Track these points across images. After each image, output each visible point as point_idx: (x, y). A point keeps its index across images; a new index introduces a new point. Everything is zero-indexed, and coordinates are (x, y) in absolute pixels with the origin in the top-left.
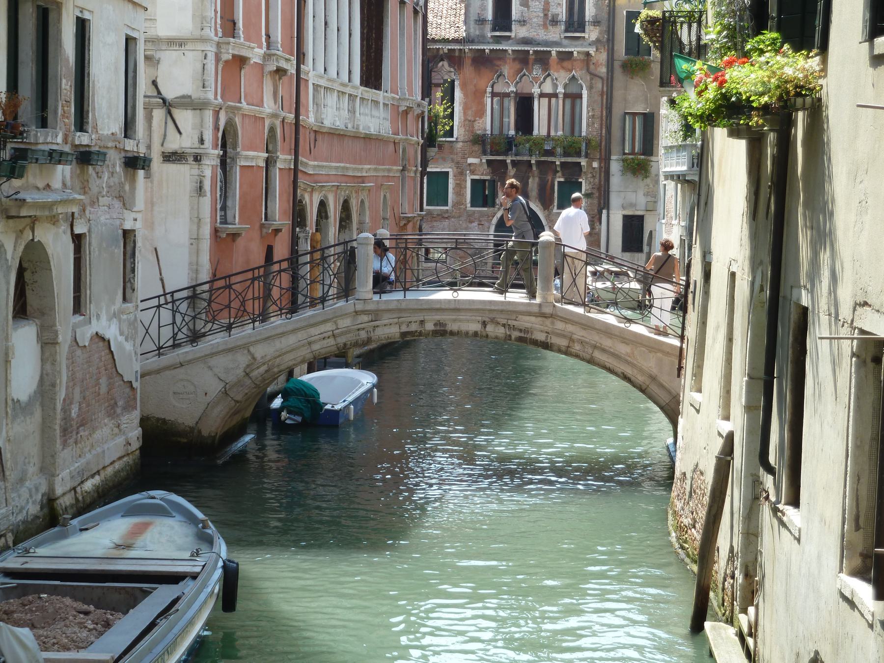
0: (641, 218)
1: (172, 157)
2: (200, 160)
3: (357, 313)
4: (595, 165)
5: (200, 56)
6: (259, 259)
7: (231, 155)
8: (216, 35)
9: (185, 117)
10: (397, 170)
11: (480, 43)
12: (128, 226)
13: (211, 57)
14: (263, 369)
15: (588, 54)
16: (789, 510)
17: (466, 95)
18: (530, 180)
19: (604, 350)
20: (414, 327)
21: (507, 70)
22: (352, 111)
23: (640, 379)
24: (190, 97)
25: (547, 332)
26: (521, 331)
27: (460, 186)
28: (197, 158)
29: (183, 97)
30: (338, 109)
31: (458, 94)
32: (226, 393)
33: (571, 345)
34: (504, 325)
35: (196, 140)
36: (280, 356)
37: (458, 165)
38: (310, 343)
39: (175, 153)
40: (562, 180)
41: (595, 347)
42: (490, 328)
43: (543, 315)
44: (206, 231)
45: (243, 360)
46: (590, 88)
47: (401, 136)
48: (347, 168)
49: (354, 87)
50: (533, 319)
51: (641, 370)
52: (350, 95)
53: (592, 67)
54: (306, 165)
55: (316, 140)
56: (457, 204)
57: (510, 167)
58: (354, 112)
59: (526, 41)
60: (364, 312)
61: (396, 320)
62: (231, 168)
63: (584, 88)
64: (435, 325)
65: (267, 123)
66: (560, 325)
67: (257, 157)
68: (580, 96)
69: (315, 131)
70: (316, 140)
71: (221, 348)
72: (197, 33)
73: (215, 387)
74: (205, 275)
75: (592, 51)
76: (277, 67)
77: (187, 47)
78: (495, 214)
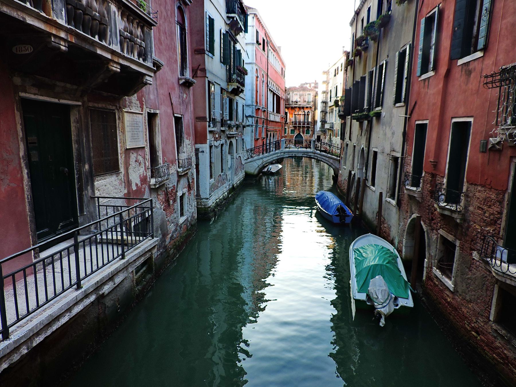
4: (312, 126)
6: (261, 144)
9: (250, 119)
13: (254, 108)
22: (275, 118)
27: (289, 131)
28: (252, 126)
31: (288, 114)
37: (288, 127)
41: (322, 158)
44: (253, 139)
45: (261, 161)
46: (311, 113)
56: (288, 134)
59: (300, 105)
60: (282, 153)
65: (263, 120)
66: (316, 155)
72: (252, 104)
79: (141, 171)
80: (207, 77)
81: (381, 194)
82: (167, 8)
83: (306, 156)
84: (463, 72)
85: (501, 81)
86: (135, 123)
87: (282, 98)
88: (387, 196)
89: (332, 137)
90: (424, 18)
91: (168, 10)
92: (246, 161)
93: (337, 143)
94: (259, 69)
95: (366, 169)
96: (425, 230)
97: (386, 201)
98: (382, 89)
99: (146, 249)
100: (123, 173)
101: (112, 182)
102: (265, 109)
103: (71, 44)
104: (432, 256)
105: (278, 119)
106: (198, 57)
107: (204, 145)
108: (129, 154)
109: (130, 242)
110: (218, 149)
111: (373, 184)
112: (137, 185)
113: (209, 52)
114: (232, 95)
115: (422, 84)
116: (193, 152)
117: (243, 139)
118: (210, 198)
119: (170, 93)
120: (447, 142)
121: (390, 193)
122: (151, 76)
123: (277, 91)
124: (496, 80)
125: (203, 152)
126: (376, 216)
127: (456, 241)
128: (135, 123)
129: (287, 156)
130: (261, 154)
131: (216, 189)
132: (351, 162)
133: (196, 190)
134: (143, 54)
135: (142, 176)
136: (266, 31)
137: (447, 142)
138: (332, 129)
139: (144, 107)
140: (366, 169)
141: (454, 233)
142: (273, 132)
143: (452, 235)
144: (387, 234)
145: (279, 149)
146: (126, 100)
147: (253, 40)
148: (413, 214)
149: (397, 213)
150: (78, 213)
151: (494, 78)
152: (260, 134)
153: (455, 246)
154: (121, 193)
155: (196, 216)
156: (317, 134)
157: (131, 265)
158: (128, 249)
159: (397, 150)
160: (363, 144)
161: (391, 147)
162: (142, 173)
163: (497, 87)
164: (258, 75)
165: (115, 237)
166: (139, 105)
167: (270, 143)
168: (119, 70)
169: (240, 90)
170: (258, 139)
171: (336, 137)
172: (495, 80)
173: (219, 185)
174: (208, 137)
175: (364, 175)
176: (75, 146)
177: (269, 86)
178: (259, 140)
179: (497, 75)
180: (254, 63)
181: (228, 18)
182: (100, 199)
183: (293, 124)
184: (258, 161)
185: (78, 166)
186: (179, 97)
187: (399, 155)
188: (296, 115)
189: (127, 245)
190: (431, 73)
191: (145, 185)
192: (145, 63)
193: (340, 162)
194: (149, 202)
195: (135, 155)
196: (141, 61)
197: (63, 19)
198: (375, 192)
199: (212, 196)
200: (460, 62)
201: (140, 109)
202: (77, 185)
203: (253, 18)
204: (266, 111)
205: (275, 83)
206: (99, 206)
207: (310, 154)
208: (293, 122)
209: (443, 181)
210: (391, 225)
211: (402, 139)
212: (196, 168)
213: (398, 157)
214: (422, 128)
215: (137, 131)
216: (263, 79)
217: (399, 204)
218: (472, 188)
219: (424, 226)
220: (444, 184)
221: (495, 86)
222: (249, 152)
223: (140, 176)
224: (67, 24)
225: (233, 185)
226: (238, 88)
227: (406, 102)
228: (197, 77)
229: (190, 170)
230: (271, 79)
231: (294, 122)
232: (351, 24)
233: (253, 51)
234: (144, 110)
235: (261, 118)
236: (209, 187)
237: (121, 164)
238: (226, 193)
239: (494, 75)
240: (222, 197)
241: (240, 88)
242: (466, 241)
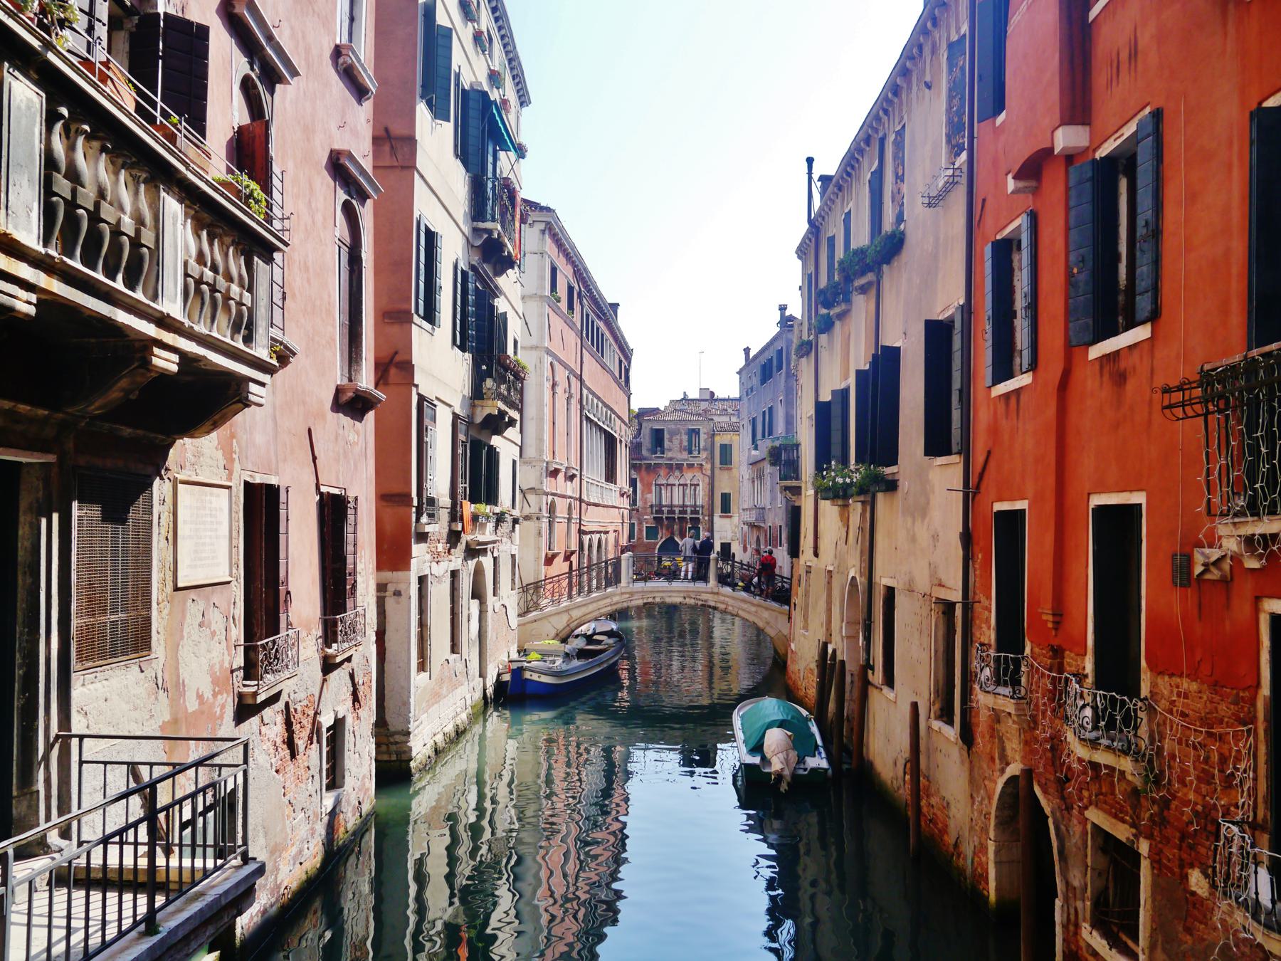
0: (729, 544)
1: (527, 518)
3: (622, 594)
4: (707, 518)
11: (648, 460)
15: (701, 465)
17: (643, 485)
19: (744, 610)
20: (650, 600)
21: (662, 472)
27: (640, 530)
31: (639, 485)
37: (639, 519)
42: (687, 600)
43: (712, 593)
53: (704, 472)
56: (639, 539)
59: (671, 459)
68: (698, 485)
75: (704, 463)
79: (215, 654)
80: (417, 386)
81: (915, 706)
82: (313, 205)
84: (1106, 377)
85: (1205, 401)
86: (208, 512)
87: (621, 441)
88: (932, 715)
90: (990, 245)
91: (317, 210)
95: (868, 639)
96: (1047, 811)
99: (223, 899)
100: (162, 660)
101: (126, 687)
102: (575, 472)
103: (43, 297)
104: (1075, 888)
106: (395, 330)
107: (400, 574)
108: (184, 603)
109: (174, 876)
110: (443, 584)
111: (889, 680)
112: (200, 697)
113: (424, 318)
114: (486, 432)
115: (1001, 407)
116: (370, 595)
119: (310, 431)
120: (1084, 560)
121: (937, 706)
122: (263, 385)
124: (1194, 399)
126: (905, 773)
127: (1138, 840)
128: (208, 512)
130: (565, 598)
131: (433, 704)
132: (823, 617)
134: (245, 326)
135: (217, 666)
136: (576, 266)
137: (1084, 560)
139: (237, 466)
140: (868, 639)
141: (1131, 817)
142: (598, 536)
143: (1123, 821)
144: (940, 825)
146: (186, 449)
148: (1008, 764)
149: (962, 762)
150: (14, 787)
151: (1187, 393)
153: (1137, 856)
154: (152, 722)
156: (721, 539)
157: (172, 952)
158: (167, 899)
159: (950, 583)
160: (854, 566)
161: (931, 576)
162: (216, 661)
163: (1199, 415)
165: (128, 861)
166: (222, 463)
167: (579, 569)
168: (174, 368)
169: (507, 420)
172: (1190, 399)
173: (444, 691)
175: (862, 655)
176: (24, 581)
179: (1194, 385)
181: (476, 231)
182: (85, 740)
183: (652, 513)
184: (556, 618)
185: (27, 641)
186: (336, 439)
187: (956, 596)
188: (660, 485)
189: (164, 887)
190: (1023, 380)
191: (225, 695)
192: (248, 347)
194: (241, 747)
195: (201, 605)
196: (240, 345)
197: (30, 231)
198: (895, 702)
200: (1096, 352)
201: (224, 474)
202: (19, 698)
203: (543, 232)
204: (578, 476)
206: (81, 763)
208: (651, 506)
209: (1084, 668)
210: (948, 797)
211: (960, 552)
212: (377, 642)
213: (954, 604)
214: (1010, 524)
215: (211, 537)
217: (967, 736)
218: (1164, 683)
219: (1043, 802)
220: (1086, 676)
221: (1190, 413)
222: (531, 591)
223: (211, 667)
224: (41, 243)
227: (965, 452)
228: (386, 384)
229: (360, 648)
230: (589, 389)
231: (656, 506)
232: (802, 252)
234: (235, 475)
237: (158, 633)
239: (1185, 387)
241: (507, 413)
242: (1167, 840)
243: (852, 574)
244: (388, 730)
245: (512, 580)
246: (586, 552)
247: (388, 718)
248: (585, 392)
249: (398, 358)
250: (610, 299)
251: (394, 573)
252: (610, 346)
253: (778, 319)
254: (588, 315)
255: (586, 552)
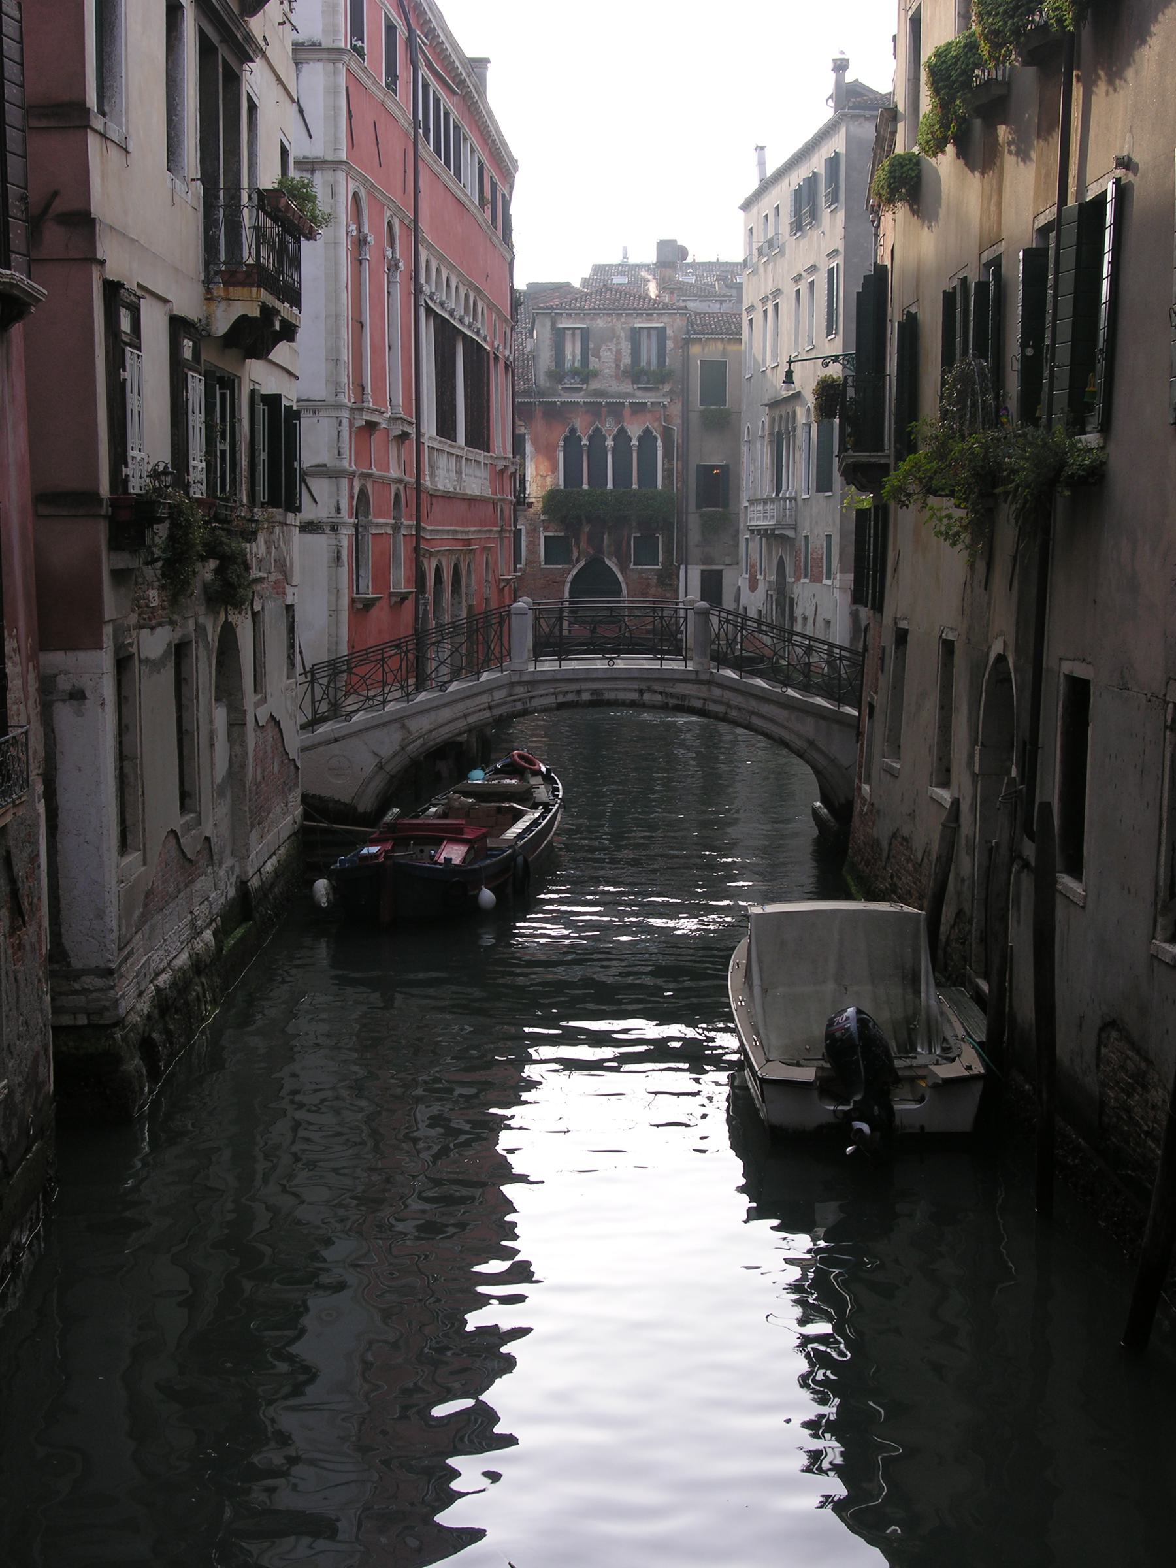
2: (337, 529)
5: (335, 422)
7: (363, 524)
8: (349, 401)
10: (497, 531)
11: (549, 396)
12: (289, 603)
13: (345, 422)
14: (420, 741)
16: (1066, 881)
18: (605, 537)
20: (570, 698)
22: (459, 472)
23: (799, 744)
24: (325, 465)
25: (705, 700)
26: (678, 699)
27: (533, 544)
28: (335, 528)
29: (318, 466)
30: (448, 470)
32: (381, 768)
33: (729, 711)
34: (661, 693)
35: (333, 510)
36: (434, 730)
38: (465, 716)
39: (311, 523)
40: (638, 535)
41: (752, 713)
42: (646, 696)
44: (345, 602)
47: (499, 496)
48: (456, 532)
49: (460, 448)
50: (690, 686)
51: (799, 735)
52: (457, 456)
54: (425, 529)
55: (431, 504)
56: (529, 562)
57: (584, 522)
58: (461, 473)
60: (519, 683)
61: (552, 690)
62: (363, 536)
63: (659, 441)
64: (591, 694)
65: (394, 488)
67: (386, 524)
69: (431, 495)
70: (431, 504)
71: (375, 723)
72: (331, 400)
73: (369, 764)
74: (344, 650)
76: (403, 431)
77: (321, 414)
78: (570, 570)
80: (102, 263)
83: (658, 698)
87: (496, 358)
88: (1159, 933)
89: (790, 580)
92: (307, 737)
93: (824, 614)
94: (370, 195)
97: (1154, 957)
98: (1102, 333)
105: (476, 483)
107: (83, 657)
117: (290, 608)
118: (124, 969)
123: (466, 320)
125: (78, 695)
129: (551, 701)
132: (933, 734)
133: (46, 923)
138: (790, 533)
145: (501, 660)
147: (336, 32)
152: (381, 577)
155: (48, 1073)
160: (1001, 633)
164: (366, 230)
170: (369, 605)
171: (817, 579)
174: (109, 612)
177: (426, 289)
178: (374, 611)
180: (341, 162)
193: (859, 734)
198: (1083, 907)
199: (131, 953)
204: (414, 436)
205: (460, 275)
207: (681, 689)
216: (389, 253)
225: (242, 885)
226: (268, 313)
230: (429, 247)
233: (333, 92)
235: (385, 483)
236: (115, 902)
238: (208, 935)
240: (184, 956)
241: (278, 312)
243: (997, 648)
244: (69, 964)
245: (289, 657)
246: (429, 596)
247: (68, 944)
248: (423, 254)
249: (59, 206)
250: (471, 52)
251: (70, 654)
252: (472, 151)
253: (830, 89)
254: (426, 86)
255: (429, 596)
